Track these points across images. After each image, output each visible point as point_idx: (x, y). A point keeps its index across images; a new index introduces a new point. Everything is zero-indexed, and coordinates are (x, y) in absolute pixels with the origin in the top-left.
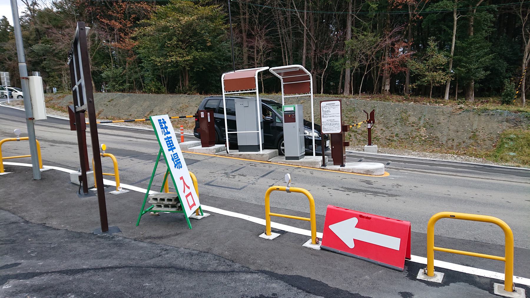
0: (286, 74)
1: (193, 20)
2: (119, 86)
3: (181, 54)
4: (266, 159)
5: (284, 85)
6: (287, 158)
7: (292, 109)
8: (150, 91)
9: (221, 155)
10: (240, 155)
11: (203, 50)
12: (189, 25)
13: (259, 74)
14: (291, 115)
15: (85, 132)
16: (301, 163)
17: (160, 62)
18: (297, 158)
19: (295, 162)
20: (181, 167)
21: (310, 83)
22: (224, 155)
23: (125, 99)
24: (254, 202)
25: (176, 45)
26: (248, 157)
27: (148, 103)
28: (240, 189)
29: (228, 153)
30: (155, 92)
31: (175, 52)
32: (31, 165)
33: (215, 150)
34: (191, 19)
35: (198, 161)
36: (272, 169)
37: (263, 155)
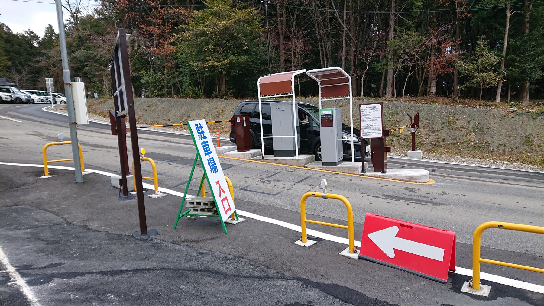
2: (158, 91)
4: (302, 165)
6: (324, 164)
8: (188, 96)
9: (256, 160)
10: (276, 160)
11: (239, 54)
12: (226, 29)
13: (296, 77)
16: (339, 168)
17: (197, 67)
18: (335, 164)
21: (348, 85)
22: (260, 160)
23: (164, 104)
26: (284, 162)
29: (263, 158)
31: (212, 56)
32: (73, 169)
33: (250, 155)
35: (234, 166)
37: (299, 160)
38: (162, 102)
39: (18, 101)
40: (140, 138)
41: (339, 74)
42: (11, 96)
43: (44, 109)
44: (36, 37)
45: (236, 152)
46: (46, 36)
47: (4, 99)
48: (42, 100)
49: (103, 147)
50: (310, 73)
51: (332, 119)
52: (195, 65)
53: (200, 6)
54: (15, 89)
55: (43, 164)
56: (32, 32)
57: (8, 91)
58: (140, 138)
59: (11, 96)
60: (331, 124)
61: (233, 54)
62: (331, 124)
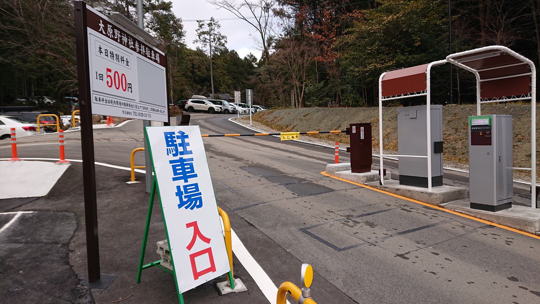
0: (488, 62)
1: (397, 18)
2: (319, 100)
3: (382, 60)
4: (436, 202)
5: (482, 84)
6: (474, 206)
7: (486, 122)
8: (348, 105)
9: (372, 186)
10: (397, 190)
11: (411, 53)
12: (396, 24)
13: (432, 68)
14: (484, 133)
15: (82, 140)
16: (498, 217)
17: (359, 71)
18: (492, 208)
19: (487, 215)
20: (200, 206)
21: (530, 78)
22: (376, 187)
23: (319, 113)
24: (339, 284)
25: (378, 50)
26: (409, 194)
27: (338, 117)
28: (339, 250)
29: (381, 184)
30: (353, 106)
31: (376, 59)
32: (144, 172)
33: (365, 179)
34: (395, 17)
35: (332, 190)
36: (434, 221)
37: (431, 194)
38: (318, 111)
39: (226, 112)
40: (78, 139)
41: (505, 58)
42: (221, 108)
43: (230, 119)
44: (255, 59)
45: (349, 172)
46: (262, 58)
47: (216, 110)
48: (245, 111)
49: (226, 155)
50: (453, 58)
51: (490, 134)
52: (357, 69)
53: (374, 5)
54: (226, 102)
55: (130, 167)
56: (252, 56)
57: (221, 103)
58: (78, 139)
59: (221, 108)
60: (488, 142)
61: (403, 54)
62: (488, 142)
